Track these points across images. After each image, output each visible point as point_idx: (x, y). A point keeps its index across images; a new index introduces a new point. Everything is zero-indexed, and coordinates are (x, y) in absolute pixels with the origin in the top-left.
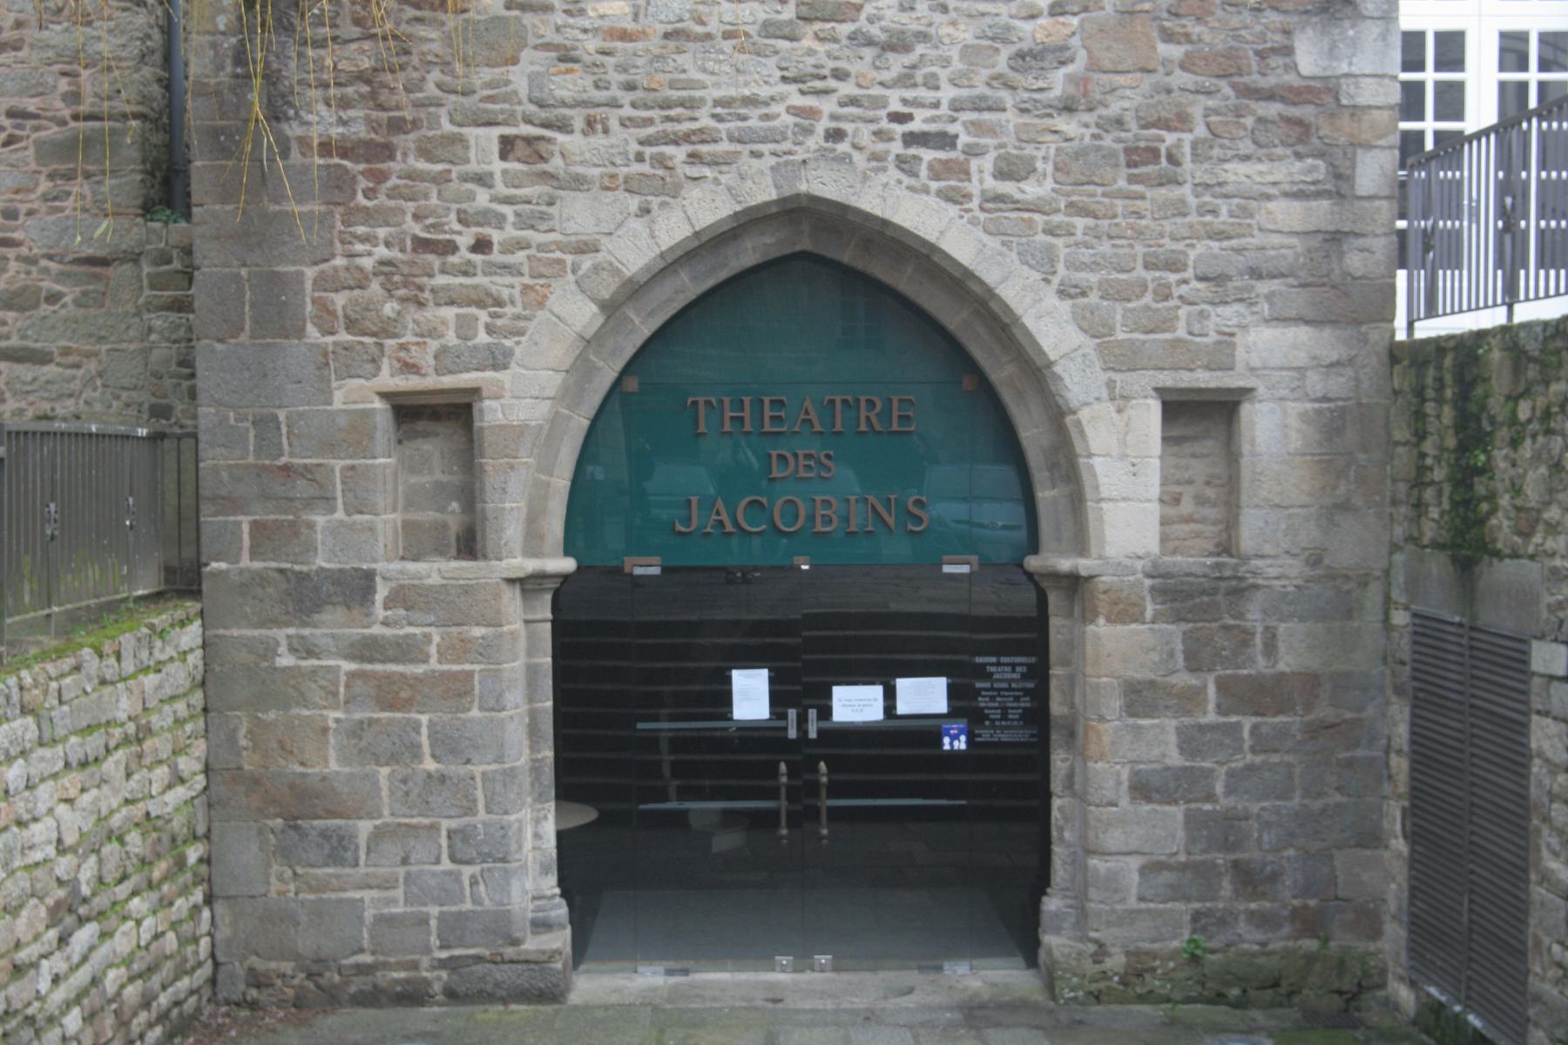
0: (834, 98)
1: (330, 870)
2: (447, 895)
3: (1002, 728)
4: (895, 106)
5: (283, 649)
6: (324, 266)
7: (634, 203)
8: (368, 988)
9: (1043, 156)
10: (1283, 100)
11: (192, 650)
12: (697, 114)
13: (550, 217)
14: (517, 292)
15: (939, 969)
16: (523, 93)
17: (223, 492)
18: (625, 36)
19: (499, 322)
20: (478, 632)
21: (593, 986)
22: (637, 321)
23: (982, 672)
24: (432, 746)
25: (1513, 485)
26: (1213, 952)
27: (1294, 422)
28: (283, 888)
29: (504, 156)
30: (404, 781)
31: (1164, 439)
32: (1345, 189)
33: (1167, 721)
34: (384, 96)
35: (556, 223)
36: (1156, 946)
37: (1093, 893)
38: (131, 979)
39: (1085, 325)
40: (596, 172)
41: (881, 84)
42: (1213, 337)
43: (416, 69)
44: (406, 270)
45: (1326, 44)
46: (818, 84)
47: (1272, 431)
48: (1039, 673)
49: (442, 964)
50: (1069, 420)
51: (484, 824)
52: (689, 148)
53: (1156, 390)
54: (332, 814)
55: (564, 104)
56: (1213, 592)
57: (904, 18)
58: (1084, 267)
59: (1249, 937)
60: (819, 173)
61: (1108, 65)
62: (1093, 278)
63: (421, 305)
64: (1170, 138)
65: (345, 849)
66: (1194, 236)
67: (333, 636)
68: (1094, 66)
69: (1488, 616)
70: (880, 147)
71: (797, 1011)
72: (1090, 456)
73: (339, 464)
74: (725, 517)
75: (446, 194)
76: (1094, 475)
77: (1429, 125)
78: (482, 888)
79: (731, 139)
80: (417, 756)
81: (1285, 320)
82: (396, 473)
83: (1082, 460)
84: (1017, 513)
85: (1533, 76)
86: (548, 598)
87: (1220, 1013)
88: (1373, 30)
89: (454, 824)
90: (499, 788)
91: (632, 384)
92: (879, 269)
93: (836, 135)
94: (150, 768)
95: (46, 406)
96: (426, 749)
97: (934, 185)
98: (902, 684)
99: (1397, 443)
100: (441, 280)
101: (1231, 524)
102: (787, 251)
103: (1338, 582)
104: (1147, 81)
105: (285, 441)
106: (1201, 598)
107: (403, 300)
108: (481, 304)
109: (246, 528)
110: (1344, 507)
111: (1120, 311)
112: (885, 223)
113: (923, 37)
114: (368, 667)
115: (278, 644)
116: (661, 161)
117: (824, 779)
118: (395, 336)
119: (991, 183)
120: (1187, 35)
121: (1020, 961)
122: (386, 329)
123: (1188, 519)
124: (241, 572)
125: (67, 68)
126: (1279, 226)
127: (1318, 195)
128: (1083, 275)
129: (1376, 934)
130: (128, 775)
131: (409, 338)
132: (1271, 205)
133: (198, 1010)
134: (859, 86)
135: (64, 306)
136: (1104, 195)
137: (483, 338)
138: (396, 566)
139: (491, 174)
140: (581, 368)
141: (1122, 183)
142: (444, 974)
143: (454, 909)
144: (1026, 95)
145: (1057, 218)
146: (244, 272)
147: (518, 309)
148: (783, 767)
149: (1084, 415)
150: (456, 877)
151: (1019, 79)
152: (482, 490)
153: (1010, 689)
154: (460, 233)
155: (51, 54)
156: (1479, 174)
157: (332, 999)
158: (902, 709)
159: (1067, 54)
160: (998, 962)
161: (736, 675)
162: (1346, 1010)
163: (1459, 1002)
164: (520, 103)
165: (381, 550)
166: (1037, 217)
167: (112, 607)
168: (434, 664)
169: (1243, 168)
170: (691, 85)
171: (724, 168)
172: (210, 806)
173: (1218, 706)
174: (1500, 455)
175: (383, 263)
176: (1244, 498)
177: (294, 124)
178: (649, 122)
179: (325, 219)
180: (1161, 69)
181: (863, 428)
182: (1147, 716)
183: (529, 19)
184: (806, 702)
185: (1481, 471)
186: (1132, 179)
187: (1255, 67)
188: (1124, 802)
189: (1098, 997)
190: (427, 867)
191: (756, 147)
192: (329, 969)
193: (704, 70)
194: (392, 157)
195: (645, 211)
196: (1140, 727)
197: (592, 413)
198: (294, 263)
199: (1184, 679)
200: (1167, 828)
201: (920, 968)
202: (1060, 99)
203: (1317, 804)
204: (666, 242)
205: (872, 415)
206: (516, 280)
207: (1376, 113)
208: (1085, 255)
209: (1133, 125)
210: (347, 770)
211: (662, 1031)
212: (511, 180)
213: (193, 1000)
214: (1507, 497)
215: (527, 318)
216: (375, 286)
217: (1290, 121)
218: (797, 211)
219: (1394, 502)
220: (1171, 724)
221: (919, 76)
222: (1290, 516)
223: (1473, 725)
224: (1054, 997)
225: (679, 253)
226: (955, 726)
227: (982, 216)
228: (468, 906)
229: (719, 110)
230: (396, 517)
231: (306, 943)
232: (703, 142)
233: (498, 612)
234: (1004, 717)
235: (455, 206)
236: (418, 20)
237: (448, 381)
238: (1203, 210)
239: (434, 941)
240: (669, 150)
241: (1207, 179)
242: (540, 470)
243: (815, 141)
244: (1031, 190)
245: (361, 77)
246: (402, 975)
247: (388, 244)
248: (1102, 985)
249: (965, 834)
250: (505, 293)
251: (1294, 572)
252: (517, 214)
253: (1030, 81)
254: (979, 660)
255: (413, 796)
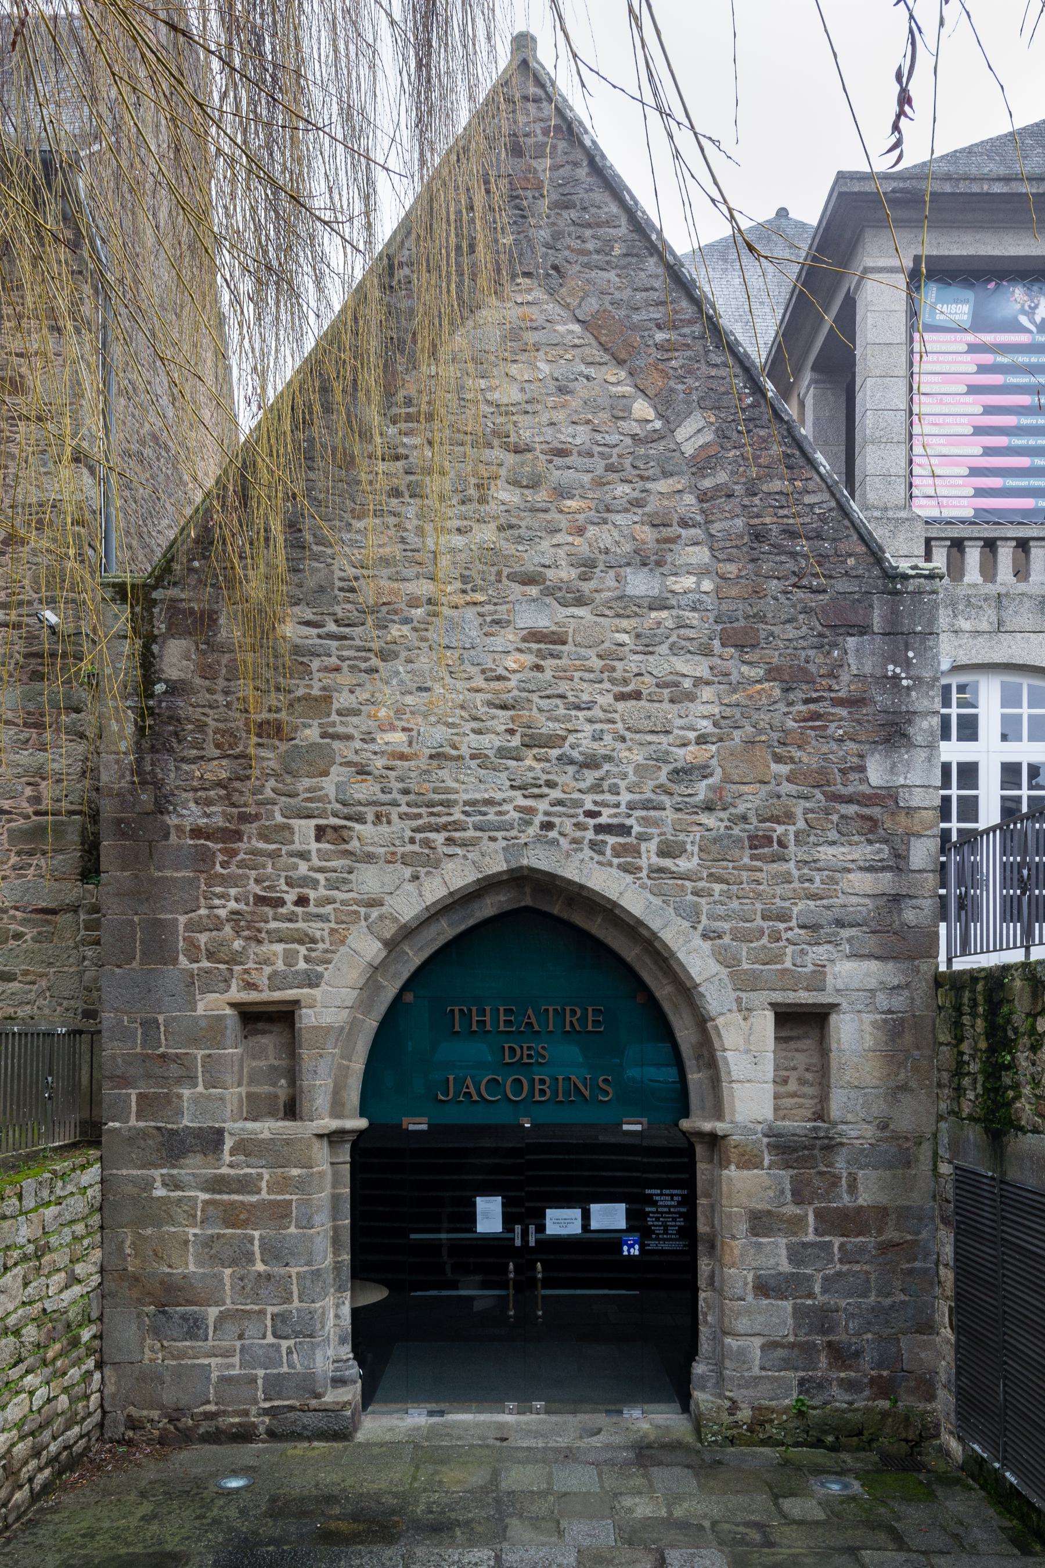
0: (547, 800)
1: (187, 1343)
2: (271, 1358)
3: (664, 1240)
4: (589, 806)
5: (158, 1184)
6: (193, 915)
7: (408, 872)
8: (212, 1429)
9: (692, 840)
10: (858, 803)
11: (91, 1186)
12: (452, 811)
13: (350, 882)
14: (326, 933)
15: (620, 1412)
16: (332, 796)
17: (118, 1073)
18: (402, 757)
19: (313, 954)
20: (295, 1172)
21: (378, 1426)
22: (411, 953)
23: (650, 1201)
24: (262, 1253)
25: (1034, 1079)
26: (814, 1408)
27: (868, 1028)
28: (154, 1356)
29: (318, 839)
30: (241, 1279)
31: (776, 1038)
32: (902, 864)
33: (779, 1240)
34: (236, 797)
35: (353, 886)
36: (774, 1403)
37: (728, 1363)
38: (22, 1438)
39: (721, 959)
40: (382, 850)
41: (579, 790)
42: (811, 968)
43: (257, 779)
44: (249, 918)
45: (888, 765)
46: (536, 791)
47: (852, 1034)
48: (690, 1201)
49: (266, 1412)
50: (709, 1025)
51: (298, 1310)
52: (447, 834)
53: (770, 1004)
54: (189, 1303)
55: (360, 803)
56: (812, 1147)
57: (595, 745)
58: (720, 918)
59: (840, 1398)
60: (536, 852)
61: (737, 779)
62: (727, 926)
63: (259, 942)
64: (780, 829)
65: (199, 1328)
66: (796, 897)
67: (193, 1175)
68: (727, 779)
69: (1013, 1174)
70: (579, 834)
71: (517, 1448)
72: (725, 1050)
73: (200, 1053)
74: (472, 1090)
75: (278, 865)
76: (727, 1064)
77: (954, 825)
78: (295, 1356)
79: (477, 828)
80: (251, 1261)
81: (861, 956)
82: (242, 1060)
83: (718, 1053)
84: (672, 1074)
85: (1025, 793)
86: (348, 1146)
87: (819, 1456)
88: (922, 754)
89: (276, 1309)
90: (308, 1283)
91: (409, 997)
92: (579, 919)
93: (548, 826)
94: (48, 1276)
95: (11, 1011)
96: (258, 1256)
97: (616, 861)
98: (594, 1207)
99: (941, 1044)
100: (273, 925)
101: (824, 1098)
102: (515, 906)
103: (900, 1142)
104: (765, 789)
105: (163, 1037)
106: (804, 1152)
107: (247, 939)
108: (301, 942)
109: (134, 1098)
110: (904, 1088)
111: (745, 949)
112: (582, 887)
113: (608, 758)
114: (218, 1197)
115: (155, 1180)
116: (427, 843)
117: (540, 1276)
118: (241, 963)
119: (655, 860)
120: (791, 758)
121: (677, 1406)
122: (235, 959)
123: (794, 1095)
124: (130, 1129)
125: (32, 780)
126: (857, 891)
127: (883, 869)
128: (719, 924)
129: (931, 1397)
130: (26, 1285)
131: (250, 965)
132: (851, 876)
133: (87, 1448)
134: (564, 792)
135: (25, 942)
136: (734, 868)
137: (302, 965)
138: (240, 1124)
139: (309, 852)
140: (371, 985)
141: (746, 860)
142: (267, 1420)
143: (275, 1371)
144: (680, 799)
145: (701, 884)
146: (136, 919)
147: (327, 946)
148: (511, 1266)
149: (720, 1021)
150: (277, 1348)
151: (674, 787)
152: (300, 1071)
153: (670, 1212)
154: (287, 892)
155: (20, 770)
156: (990, 858)
157: (186, 1437)
158: (594, 1225)
159: (708, 771)
160: (662, 1407)
161: (478, 1199)
162: (911, 1455)
163: (998, 1461)
164: (330, 803)
165: (228, 1114)
166: (687, 883)
167: (31, 1157)
168: (264, 1195)
169: (831, 850)
170: (448, 791)
171: (471, 848)
172: (103, 1297)
173: (816, 1229)
174: (1023, 1058)
175: (233, 913)
176: (832, 1081)
177: (173, 816)
178: (419, 816)
179: (193, 882)
180: (773, 781)
181: (568, 1028)
182: (765, 1236)
183: (336, 745)
184: (527, 1221)
185: (1008, 1067)
186: (753, 857)
187: (839, 781)
188: (750, 1298)
189: (732, 1441)
190: (256, 1341)
191: (492, 834)
192: (184, 1416)
193: (457, 781)
194: (240, 840)
195: (416, 878)
196: (760, 1244)
197: (380, 1018)
198: (172, 912)
199: (791, 1209)
200: (780, 1316)
201: (607, 1412)
202: (703, 801)
203: (888, 1301)
204: (430, 899)
205: (574, 1020)
206: (325, 925)
207: (924, 813)
208: (720, 910)
209: (754, 820)
210: (201, 1270)
211: (417, 1467)
212: (323, 856)
213: (82, 1443)
214: (1028, 1087)
215: (333, 952)
216: (228, 929)
217: (863, 817)
218: (521, 878)
219: (940, 1085)
220: (783, 1241)
221: (606, 785)
222: (865, 1095)
223: (1004, 1253)
224: (700, 1440)
225: (439, 907)
226: (631, 1239)
227: (649, 882)
228: (285, 1369)
229: (467, 808)
230: (243, 1090)
231: (169, 1396)
232: (456, 830)
233: (310, 1158)
234: (666, 1231)
235: (284, 874)
236: (259, 745)
237: (277, 995)
238: (803, 879)
239: (260, 1395)
240: (432, 835)
241: (806, 857)
242: (342, 1058)
243: (533, 830)
244: (683, 864)
245: (220, 784)
246: (237, 1420)
247: (237, 900)
248: (735, 1432)
249: (635, 1319)
250: (318, 934)
251: (869, 1134)
252: (327, 879)
253: (682, 789)
254: (648, 1191)
255: (248, 1289)
